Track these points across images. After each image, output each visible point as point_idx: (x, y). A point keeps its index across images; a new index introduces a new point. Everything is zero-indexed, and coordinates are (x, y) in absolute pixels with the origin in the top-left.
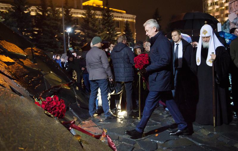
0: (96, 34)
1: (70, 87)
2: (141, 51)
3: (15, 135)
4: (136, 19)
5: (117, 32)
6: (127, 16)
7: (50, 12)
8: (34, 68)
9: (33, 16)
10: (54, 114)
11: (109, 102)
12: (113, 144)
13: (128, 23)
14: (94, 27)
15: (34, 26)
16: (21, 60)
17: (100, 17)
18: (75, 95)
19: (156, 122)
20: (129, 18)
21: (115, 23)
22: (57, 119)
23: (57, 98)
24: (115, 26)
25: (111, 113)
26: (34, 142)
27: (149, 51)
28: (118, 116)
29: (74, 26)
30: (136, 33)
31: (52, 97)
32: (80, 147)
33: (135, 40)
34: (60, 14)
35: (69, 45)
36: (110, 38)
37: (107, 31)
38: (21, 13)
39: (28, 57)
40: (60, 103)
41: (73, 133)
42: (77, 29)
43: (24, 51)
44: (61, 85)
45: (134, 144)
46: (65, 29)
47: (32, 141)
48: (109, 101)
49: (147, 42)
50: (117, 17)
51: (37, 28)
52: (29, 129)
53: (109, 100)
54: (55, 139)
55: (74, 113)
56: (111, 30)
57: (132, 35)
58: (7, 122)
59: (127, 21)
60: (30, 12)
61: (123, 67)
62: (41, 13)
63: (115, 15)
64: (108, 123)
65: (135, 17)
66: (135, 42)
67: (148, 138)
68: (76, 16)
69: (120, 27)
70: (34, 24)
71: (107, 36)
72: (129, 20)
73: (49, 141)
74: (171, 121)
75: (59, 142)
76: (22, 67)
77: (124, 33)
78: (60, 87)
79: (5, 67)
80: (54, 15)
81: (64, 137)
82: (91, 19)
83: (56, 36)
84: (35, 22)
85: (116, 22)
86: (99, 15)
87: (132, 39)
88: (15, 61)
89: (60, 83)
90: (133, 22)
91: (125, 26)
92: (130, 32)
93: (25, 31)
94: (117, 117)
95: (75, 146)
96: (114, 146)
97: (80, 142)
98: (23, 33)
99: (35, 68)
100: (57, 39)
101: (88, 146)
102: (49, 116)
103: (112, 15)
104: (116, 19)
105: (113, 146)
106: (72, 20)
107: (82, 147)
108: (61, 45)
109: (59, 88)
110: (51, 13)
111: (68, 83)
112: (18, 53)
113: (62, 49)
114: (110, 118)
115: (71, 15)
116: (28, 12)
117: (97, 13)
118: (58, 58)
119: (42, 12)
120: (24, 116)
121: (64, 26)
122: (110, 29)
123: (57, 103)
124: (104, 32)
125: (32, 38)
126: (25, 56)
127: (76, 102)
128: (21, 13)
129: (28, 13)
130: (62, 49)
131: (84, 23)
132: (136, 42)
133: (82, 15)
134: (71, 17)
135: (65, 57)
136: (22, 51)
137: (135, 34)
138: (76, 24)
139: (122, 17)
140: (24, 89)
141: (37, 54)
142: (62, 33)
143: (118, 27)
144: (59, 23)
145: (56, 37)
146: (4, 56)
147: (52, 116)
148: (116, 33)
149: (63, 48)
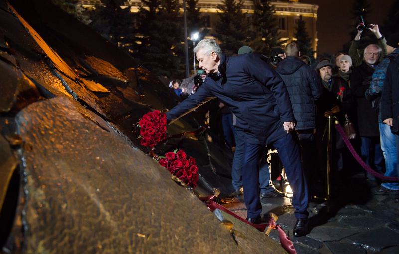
0: (242, 42)
1: (197, 137)
2: (332, 71)
3: (130, 213)
4: (318, 13)
5: (280, 38)
6: (305, 8)
7: (163, 6)
8: (139, 103)
9: (134, 14)
10: (186, 182)
11: (270, 166)
12: (290, 244)
13: (303, 20)
14: (238, 30)
15: (135, 32)
16: (119, 89)
17: (251, 11)
18: (207, 153)
19: (361, 209)
20: (305, 11)
21: (278, 21)
22: (191, 190)
23: (184, 155)
24: (277, 27)
25: (273, 186)
26: (160, 226)
27: (346, 71)
28: (286, 194)
29: (203, 29)
30: (318, 38)
31: (175, 152)
32: (234, 243)
33: (315, 52)
34: (180, 9)
35: (194, 64)
36: (268, 50)
37: (263, 37)
38: (116, 10)
39: (130, 85)
40: (189, 163)
41: (220, 217)
42: (208, 34)
43: (123, 73)
44: (183, 133)
45: (320, 247)
46: (189, 36)
47: (157, 224)
48: (269, 164)
49: (343, 55)
50: (282, 10)
51: (141, 35)
52: (150, 204)
53: (269, 162)
54: (191, 224)
55: (205, 182)
56: (270, 34)
57: (311, 42)
58: (117, 189)
59: (301, 17)
60: (130, 8)
61: (299, 101)
62: (147, 8)
63: (277, 6)
64: (268, 204)
65: (317, 8)
66: (315, 56)
67: (346, 238)
68: (206, 11)
69: (286, 28)
70: (137, 28)
71: (262, 47)
72: (305, 15)
73: (182, 227)
74: (392, 210)
75: (198, 230)
76: (120, 101)
77: (296, 40)
78: (182, 137)
79: (96, 100)
80: (169, 10)
81: (206, 222)
82: (234, 16)
83: (172, 48)
84: (138, 25)
85: (280, 20)
86: (248, 8)
87: (310, 50)
88: (110, 90)
89: (183, 129)
90: (312, 19)
91: (297, 26)
92: (307, 38)
93: (121, 41)
94: (284, 195)
95: (225, 240)
96: (292, 247)
97: (233, 234)
98: (118, 43)
99: (141, 104)
100: (174, 54)
101: (246, 242)
102: (179, 183)
103: (273, 6)
104: (279, 13)
105: (290, 247)
106: (200, 19)
107: (237, 242)
108: (181, 63)
109: (181, 139)
110: (165, 9)
111: (196, 129)
112: (114, 78)
113: (182, 71)
114: (271, 196)
115: (199, 10)
116: (127, 7)
117: (245, 4)
118: (176, 85)
119: (149, 7)
120: (141, 182)
121: (186, 28)
122: (268, 34)
123: (184, 164)
124: (256, 39)
125: (132, 52)
126: (126, 81)
127: (209, 163)
128: (116, 10)
129: (126, 8)
130: (182, 71)
131: (222, 23)
132: (317, 56)
133: (217, 9)
134: (197, 13)
135: (188, 85)
136: (120, 73)
137: (317, 40)
138: (206, 25)
139: (290, 10)
140: (127, 138)
141: (144, 78)
142: (182, 43)
143: (283, 29)
144: (178, 25)
145: (173, 50)
146: (93, 82)
147: (183, 184)
148: (279, 39)
149: (183, 69)
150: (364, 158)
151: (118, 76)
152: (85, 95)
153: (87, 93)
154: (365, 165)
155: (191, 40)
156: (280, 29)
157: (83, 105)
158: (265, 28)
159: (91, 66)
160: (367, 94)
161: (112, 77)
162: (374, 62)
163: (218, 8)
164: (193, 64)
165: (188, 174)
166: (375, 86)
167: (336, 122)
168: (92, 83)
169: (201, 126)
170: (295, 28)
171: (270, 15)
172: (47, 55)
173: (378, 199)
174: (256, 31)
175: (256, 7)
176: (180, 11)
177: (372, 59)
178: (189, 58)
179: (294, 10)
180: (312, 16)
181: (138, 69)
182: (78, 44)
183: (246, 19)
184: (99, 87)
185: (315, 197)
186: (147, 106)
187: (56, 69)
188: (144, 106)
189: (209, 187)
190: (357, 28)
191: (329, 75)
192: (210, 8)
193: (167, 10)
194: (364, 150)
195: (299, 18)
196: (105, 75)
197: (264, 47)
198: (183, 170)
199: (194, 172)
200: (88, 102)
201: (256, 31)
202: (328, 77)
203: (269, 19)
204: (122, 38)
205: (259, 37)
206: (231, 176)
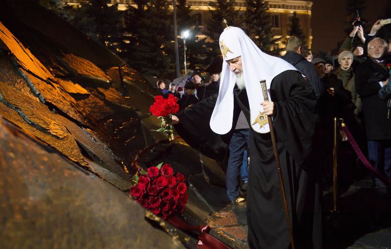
4: (313, 9)
6: (299, 5)
8: (123, 105)
16: (101, 90)
17: (243, 9)
20: (299, 8)
21: (271, 17)
24: (271, 24)
29: (194, 27)
30: (312, 36)
31: (159, 166)
34: (170, 6)
35: (185, 63)
37: (256, 35)
39: (113, 85)
46: (179, 34)
51: (129, 33)
59: (295, 13)
60: (117, 5)
62: (136, 6)
63: (270, 3)
65: (311, 5)
68: (197, 9)
69: (280, 24)
70: (124, 27)
72: (299, 11)
76: (102, 103)
80: (157, 7)
83: (162, 47)
84: (126, 23)
85: (273, 17)
86: (241, 5)
93: (108, 40)
99: (125, 106)
100: (164, 53)
102: (155, 225)
104: (272, 10)
108: (171, 62)
112: (95, 78)
113: (173, 71)
115: (189, 7)
119: (137, 4)
121: (176, 26)
123: (170, 182)
125: (120, 51)
126: (108, 81)
128: (102, 7)
130: (173, 71)
131: (213, 20)
133: (209, 7)
134: (188, 11)
136: (103, 73)
137: (311, 38)
138: (197, 22)
140: (105, 146)
142: (172, 42)
143: (277, 26)
144: (168, 22)
145: (163, 48)
146: (71, 83)
147: (163, 224)
148: (272, 37)
149: (173, 68)
151: (100, 75)
152: (57, 98)
153: (59, 96)
155: (181, 38)
156: (274, 27)
157: (51, 110)
158: (258, 25)
159: (70, 64)
161: (93, 77)
162: (380, 56)
163: (210, 5)
165: (175, 194)
167: (343, 125)
168: (69, 84)
170: (289, 25)
171: (263, 11)
172: (10, 51)
174: (248, 29)
175: (249, 3)
176: (169, 9)
178: (180, 57)
179: (287, 7)
180: (306, 13)
182: (55, 42)
183: (238, 16)
184: (78, 89)
187: (21, 67)
189: (201, 198)
190: (353, 24)
192: (201, 5)
193: (156, 7)
195: (293, 15)
198: (169, 190)
199: (182, 193)
200: (60, 106)
201: (248, 29)
203: (262, 16)
204: (109, 36)
206: (226, 185)
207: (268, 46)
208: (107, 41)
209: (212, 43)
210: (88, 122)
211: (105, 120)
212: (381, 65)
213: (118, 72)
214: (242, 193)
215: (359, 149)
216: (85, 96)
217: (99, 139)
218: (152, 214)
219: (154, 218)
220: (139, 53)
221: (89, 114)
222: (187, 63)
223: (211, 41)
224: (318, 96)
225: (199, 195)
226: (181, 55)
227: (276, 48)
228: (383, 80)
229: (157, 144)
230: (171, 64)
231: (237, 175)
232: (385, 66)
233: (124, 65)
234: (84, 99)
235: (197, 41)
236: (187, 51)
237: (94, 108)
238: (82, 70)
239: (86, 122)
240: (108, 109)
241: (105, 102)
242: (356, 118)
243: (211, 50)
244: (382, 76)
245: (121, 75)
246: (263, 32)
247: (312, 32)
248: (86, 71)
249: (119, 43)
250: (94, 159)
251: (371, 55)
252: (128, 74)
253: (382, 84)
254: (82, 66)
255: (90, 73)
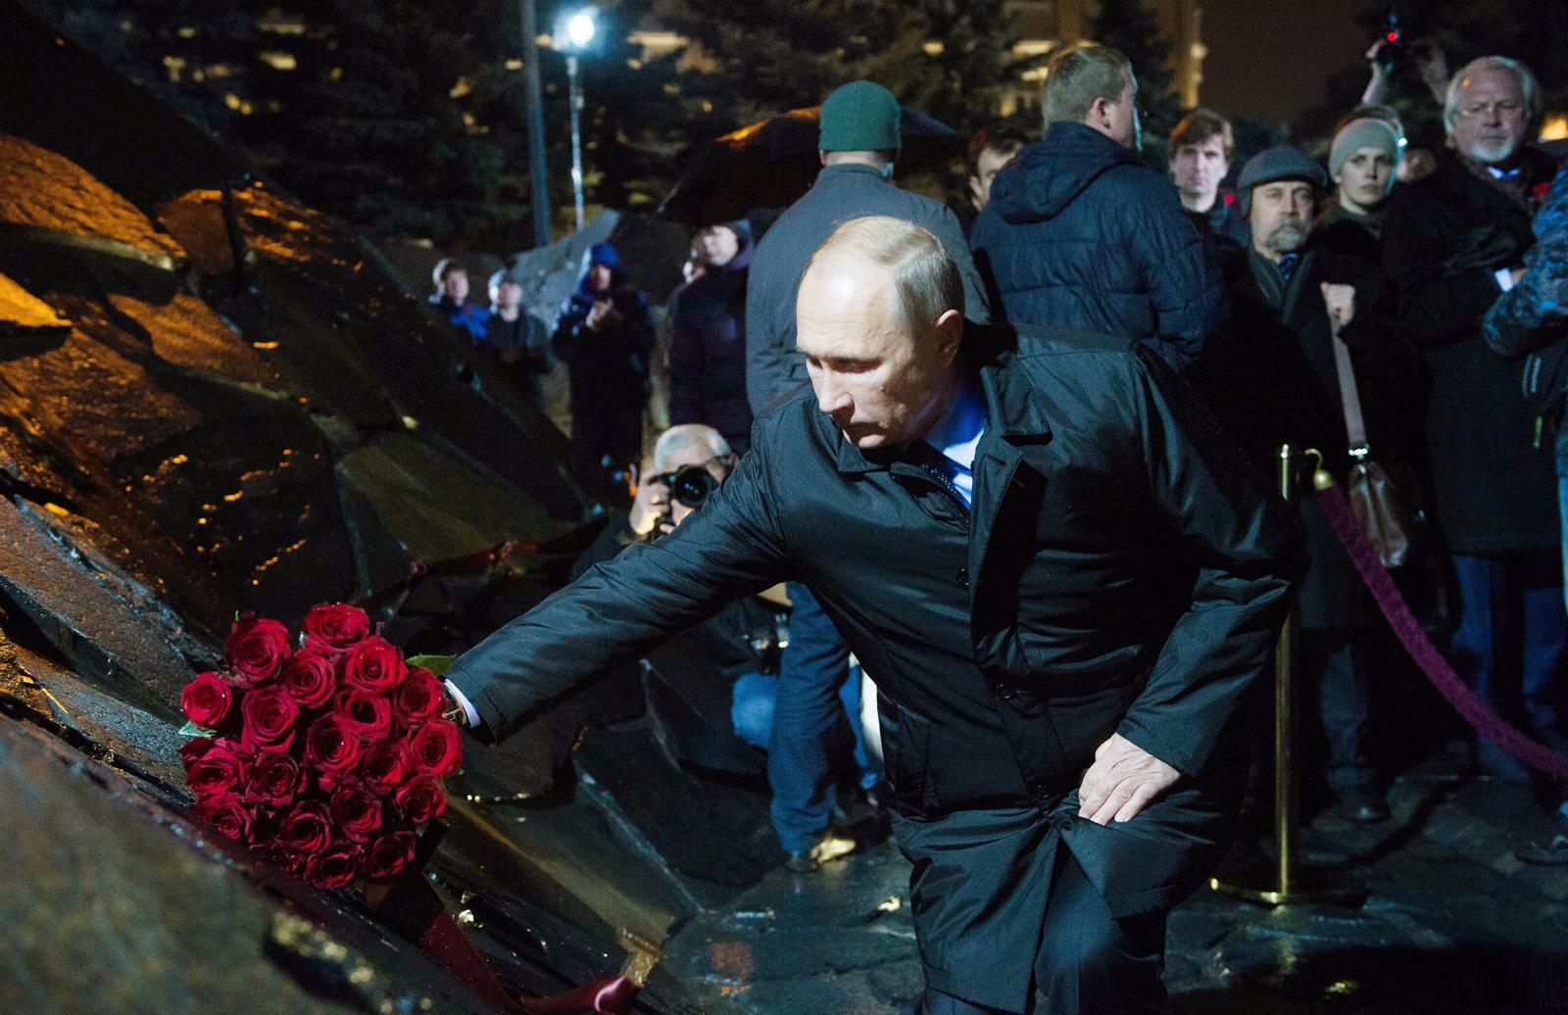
0: (823, 59)
8: (244, 386)
16: (131, 307)
30: (1205, 41)
35: (576, 175)
36: (955, 100)
37: (932, 36)
46: (544, 26)
56: (965, 20)
57: (1170, 64)
76: (132, 374)
78: (490, 570)
83: (460, 90)
88: (72, 313)
92: (1149, 42)
93: (180, 48)
100: (469, 120)
109: (485, 579)
112: (97, 244)
113: (515, 212)
122: (955, 19)
127: (642, 712)
130: (515, 212)
137: (1198, 52)
140: (141, 591)
147: (362, 975)
148: (1009, 46)
150: (1463, 663)
151: (121, 232)
154: (1468, 700)
160: (1497, 321)
161: (82, 239)
162: (1505, 150)
164: (570, 178)
166: (1554, 276)
169: (598, 509)
173: (1547, 889)
177: (1493, 132)
181: (245, 196)
185: (1215, 884)
186: (294, 399)
188: (277, 403)
191: (1297, 227)
194: (1474, 632)
196: (45, 229)
197: (933, 87)
202: (1290, 239)
205: (916, 34)
207: (986, 91)
208: (175, 55)
209: (712, 76)
210: (52, 467)
211: (150, 458)
212: (1509, 188)
213: (217, 216)
214: (840, 813)
215: (1397, 596)
216: (44, 338)
217: (109, 556)
218: (305, 927)
219: (320, 946)
220: (342, 122)
221: (63, 430)
222: (585, 172)
223: (709, 66)
224: (1192, 342)
225: (625, 828)
226: (557, 134)
227: (1028, 104)
228: (1513, 263)
229: (416, 580)
230: (507, 180)
231: (823, 726)
232: (1528, 193)
233: (250, 184)
234: (36, 351)
235: (635, 64)
236: (586, 114)
237: (86, 397)
238: (28, 206)
239: (40, 469)
240: (164, 405)
241: (148, 369)
242: (82, 518)
243: (707, 107)
244: (1508, 242)
245: (234, 223)
246: (965, 20)
247: (1205, 21)
248: (51, 210)
249: (239, 70)
250: (72, 656)
251: (1463, 148)
252: (270, 229)
253: (1505, 280)
254: (27, 186)
255: (64, 218)
